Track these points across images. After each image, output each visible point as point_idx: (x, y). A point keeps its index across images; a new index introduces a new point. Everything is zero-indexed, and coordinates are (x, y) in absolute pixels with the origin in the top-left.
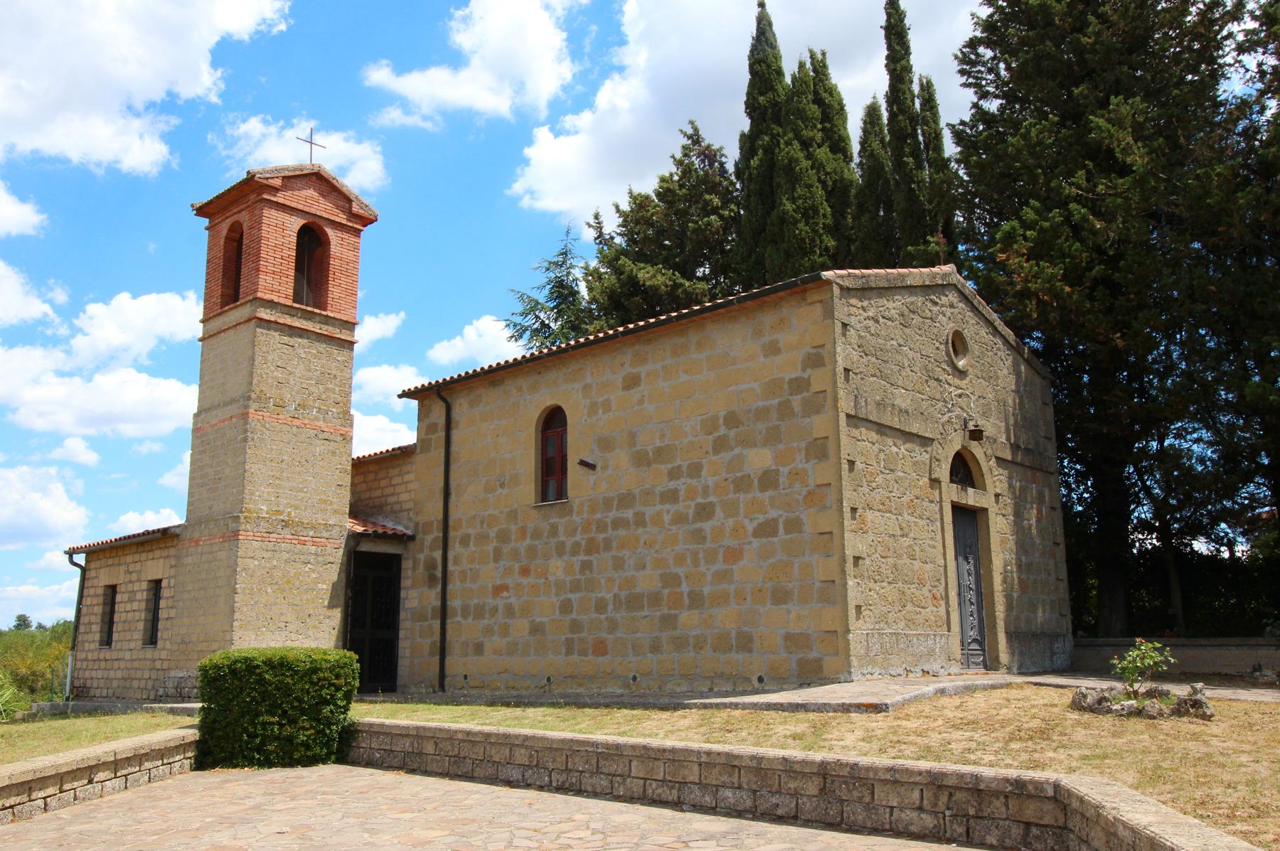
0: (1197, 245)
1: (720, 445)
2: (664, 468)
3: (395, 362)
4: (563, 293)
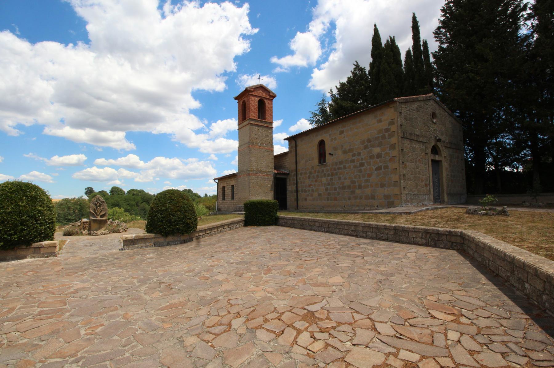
0: (510, 81)
1: (366, 147)
2: (351, 154)
3: (281, 132)
4: (323, 110)
